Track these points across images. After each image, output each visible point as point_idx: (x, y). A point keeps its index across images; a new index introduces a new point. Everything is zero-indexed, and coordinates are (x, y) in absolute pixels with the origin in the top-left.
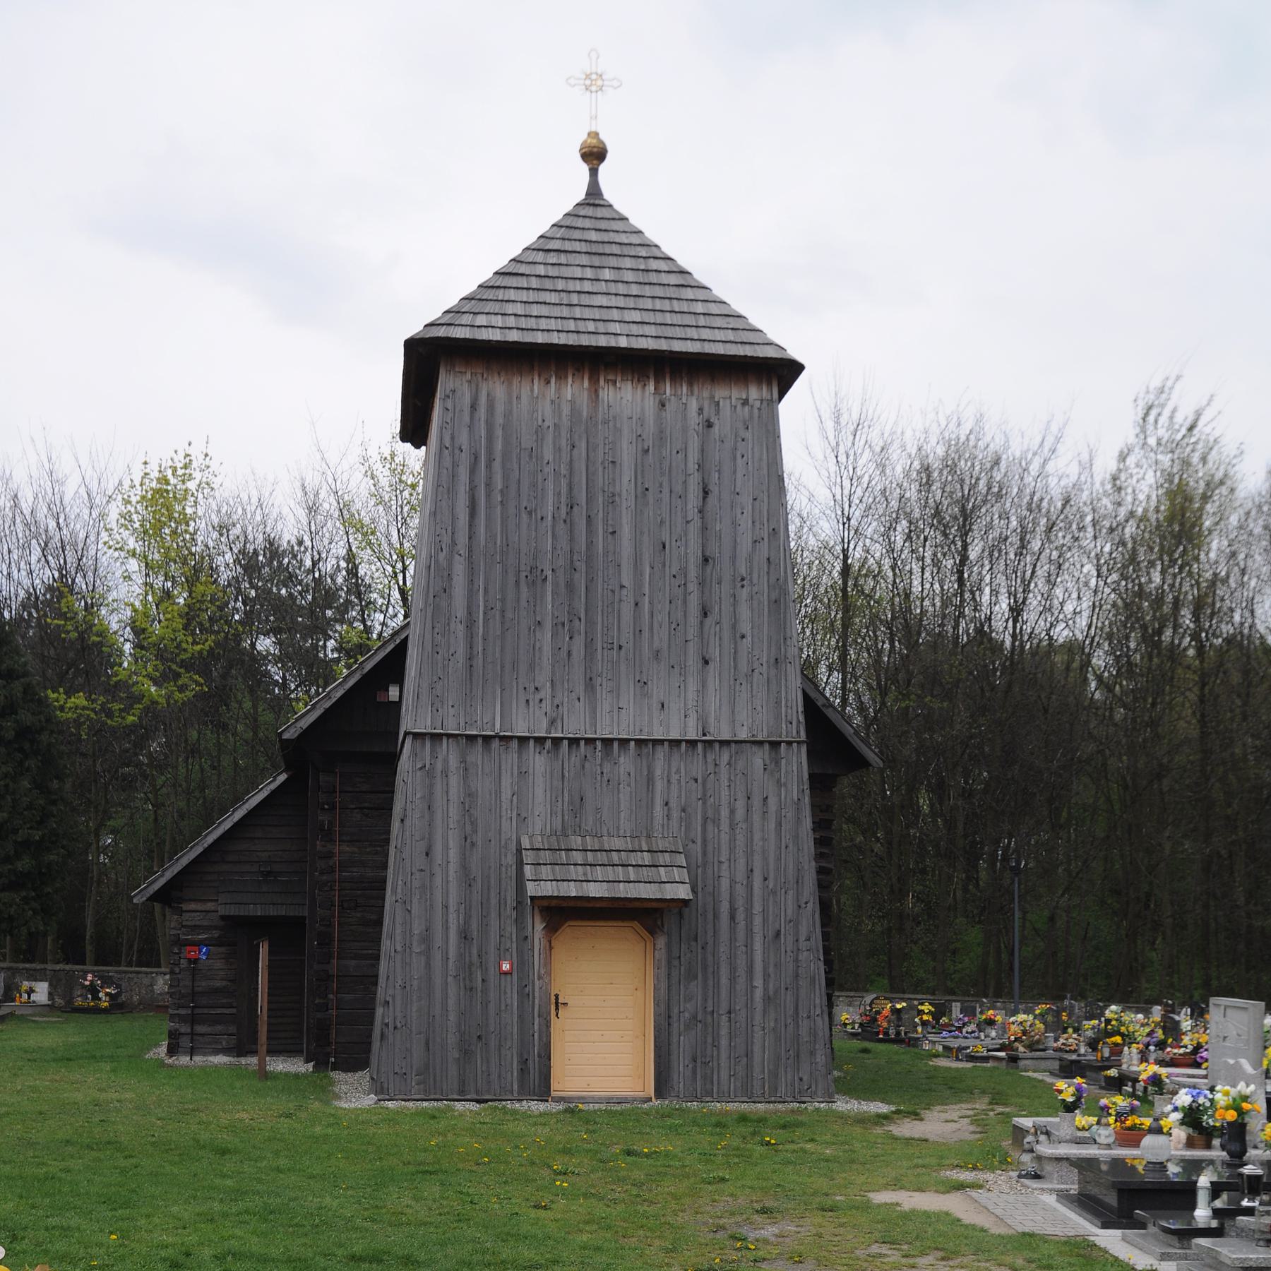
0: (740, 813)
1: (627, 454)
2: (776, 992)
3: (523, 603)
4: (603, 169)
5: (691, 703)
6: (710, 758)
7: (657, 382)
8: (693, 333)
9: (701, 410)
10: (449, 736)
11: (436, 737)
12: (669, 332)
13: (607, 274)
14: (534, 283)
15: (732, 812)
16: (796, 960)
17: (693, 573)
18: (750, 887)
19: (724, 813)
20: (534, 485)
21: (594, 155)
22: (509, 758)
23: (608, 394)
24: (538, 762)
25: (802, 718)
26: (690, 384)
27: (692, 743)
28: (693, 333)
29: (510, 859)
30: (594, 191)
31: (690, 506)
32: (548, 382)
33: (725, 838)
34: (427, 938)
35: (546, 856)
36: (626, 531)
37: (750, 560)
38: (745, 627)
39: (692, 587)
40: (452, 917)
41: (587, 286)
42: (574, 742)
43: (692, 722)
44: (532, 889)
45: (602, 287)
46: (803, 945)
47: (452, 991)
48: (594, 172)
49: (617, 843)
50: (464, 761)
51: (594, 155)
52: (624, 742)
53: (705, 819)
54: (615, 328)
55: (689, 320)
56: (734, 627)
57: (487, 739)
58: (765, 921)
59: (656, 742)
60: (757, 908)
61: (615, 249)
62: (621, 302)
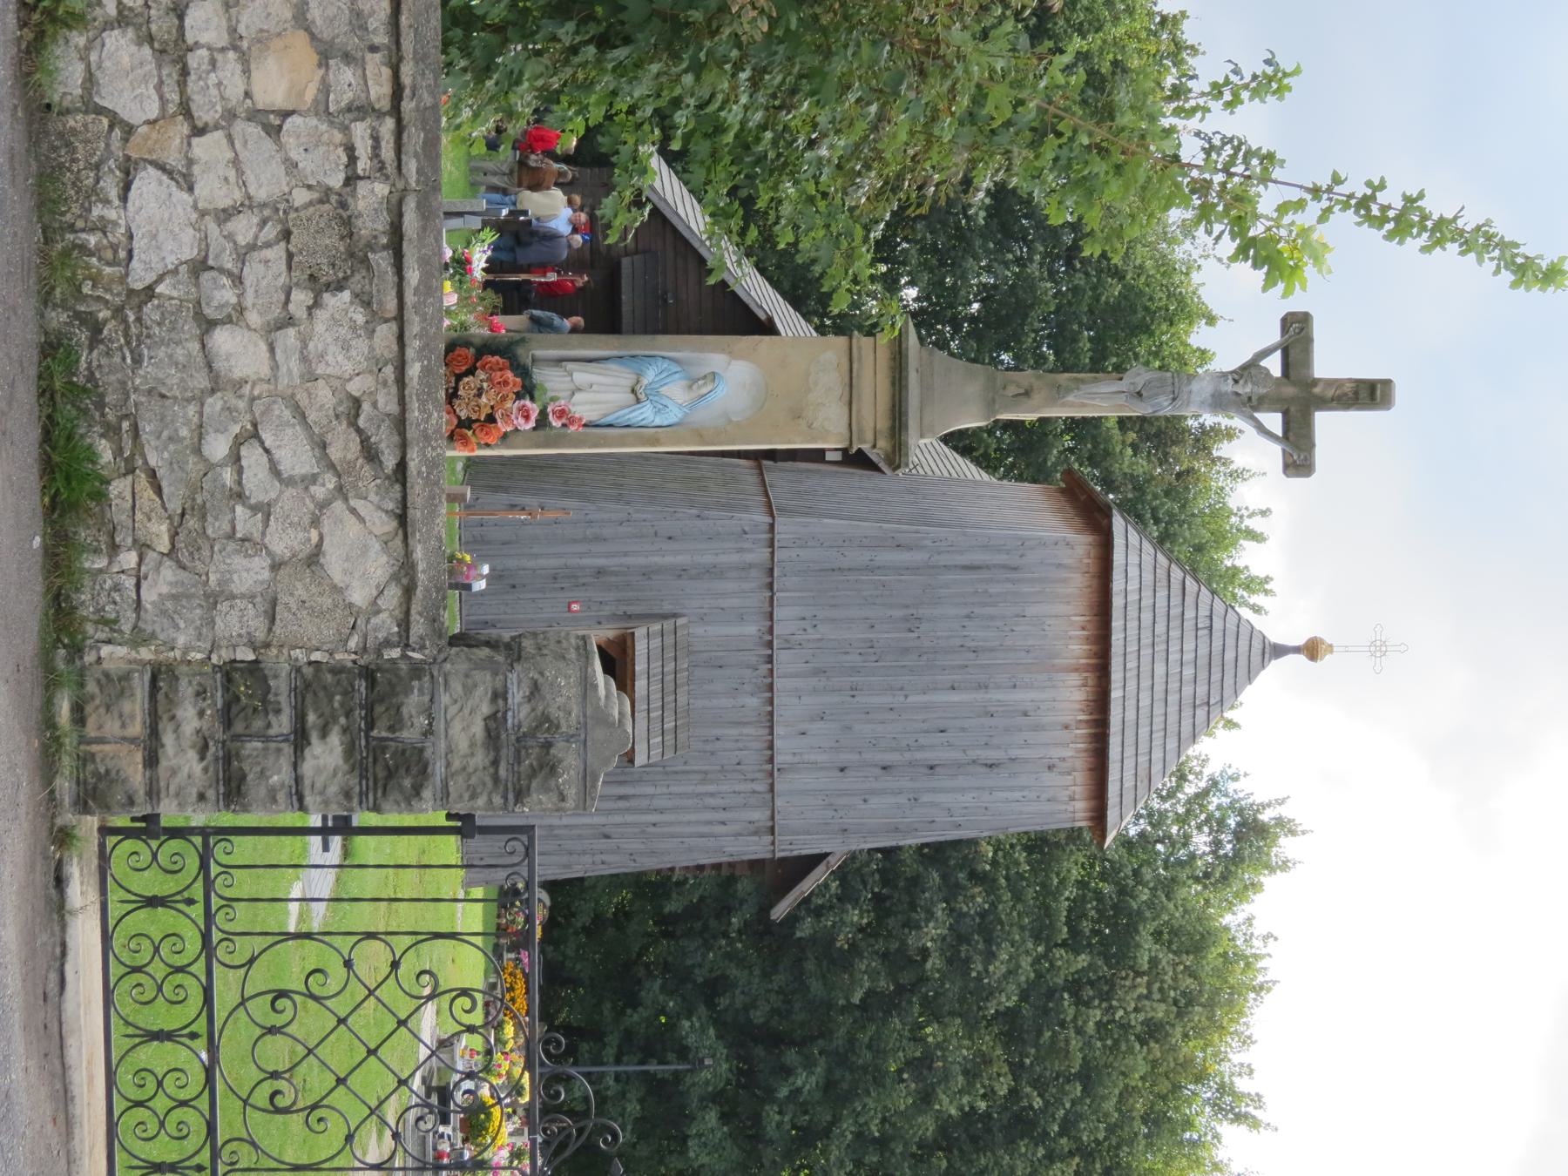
0: (712, 802)
1: (1022, 697)
2: (557, 837)
3: (890, 613)
4: (1301, 659)
5: (806, 757)
6: (758, 775)
7: (1087, 722)
8: (1130, 751)
9: (1063, 759)
10: (772, 553)
11: (771, 544)
12: (1130, 733)
13: (1188, 672)
14: (1175, 611)
15: (712, 795)
16: (584, 853)
17: (918, 755)
18: (648, 811)
19: (711, 788)
20: (992, 618)
21: (1312, 650)
22: (758, 599)
23: (1074, 679)
24: (752, 629)
25: (795, 853)
26: (1086, 751)
27: (771, 760)
28: (1130, 751)
29: (667, 608)
30: (1279, 651)
31: (979, 752)
32: (1083, 629)
33: (690, 789)
34: (598, 539)
35: (669, 640)
36: (955, 697)
37: (933, 804)
38: (875, 802)
39: (908, 756)
40: (615, 561)
41: (1174, 657)
42: (770, 659)
43: (789, 758)
44: (640, 633)
45: (1174, 669)
46: (598, 858)
47: (553, 562)
48: (1297, 650)
49: (682, 700)
50: (751, 566)
51: (1312, 650)
52: (771, 702)
53: (706, 773)
54: (1131, 685)
55: (1143, 748)
56: (873, 792)
57: (771, 586)
58: (618, 825)
59: (772, 728)
60: (630, 818)
61: (1216, 677)
62: (1159, 688)
